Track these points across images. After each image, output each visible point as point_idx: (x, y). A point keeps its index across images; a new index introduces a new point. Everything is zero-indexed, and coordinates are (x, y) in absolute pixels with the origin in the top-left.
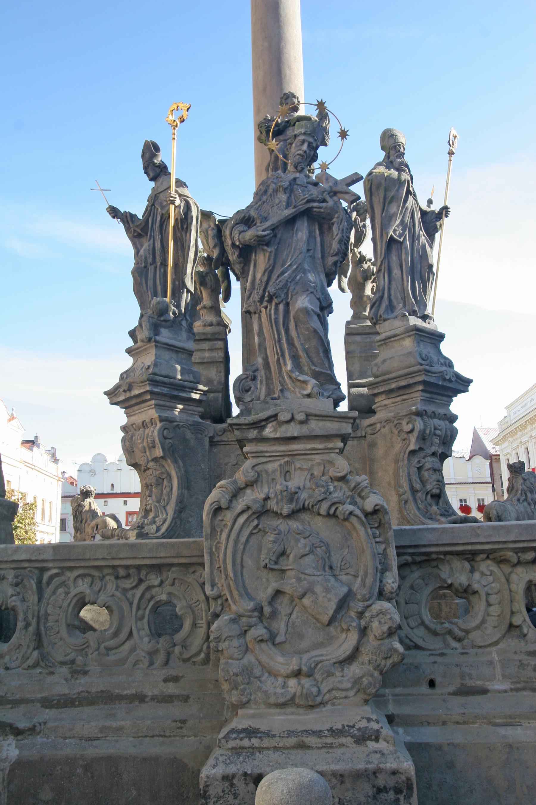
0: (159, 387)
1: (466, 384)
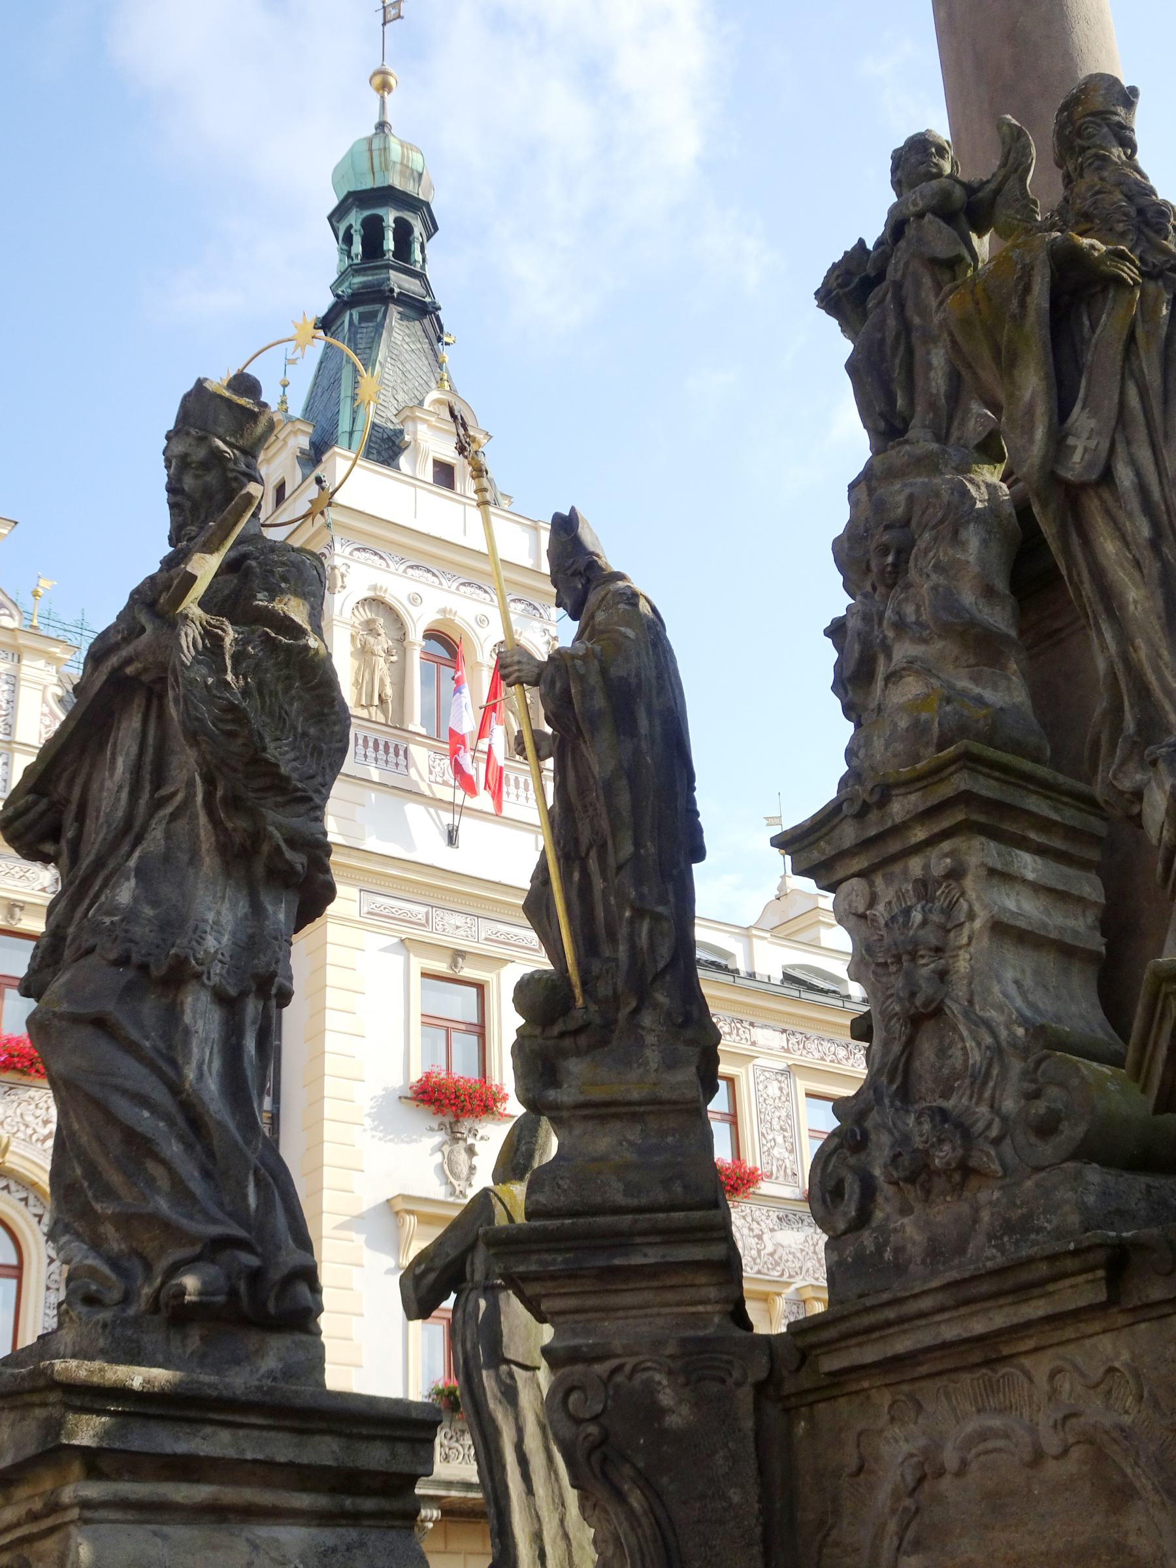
0: (535, 1257)
1: (422, 1435)
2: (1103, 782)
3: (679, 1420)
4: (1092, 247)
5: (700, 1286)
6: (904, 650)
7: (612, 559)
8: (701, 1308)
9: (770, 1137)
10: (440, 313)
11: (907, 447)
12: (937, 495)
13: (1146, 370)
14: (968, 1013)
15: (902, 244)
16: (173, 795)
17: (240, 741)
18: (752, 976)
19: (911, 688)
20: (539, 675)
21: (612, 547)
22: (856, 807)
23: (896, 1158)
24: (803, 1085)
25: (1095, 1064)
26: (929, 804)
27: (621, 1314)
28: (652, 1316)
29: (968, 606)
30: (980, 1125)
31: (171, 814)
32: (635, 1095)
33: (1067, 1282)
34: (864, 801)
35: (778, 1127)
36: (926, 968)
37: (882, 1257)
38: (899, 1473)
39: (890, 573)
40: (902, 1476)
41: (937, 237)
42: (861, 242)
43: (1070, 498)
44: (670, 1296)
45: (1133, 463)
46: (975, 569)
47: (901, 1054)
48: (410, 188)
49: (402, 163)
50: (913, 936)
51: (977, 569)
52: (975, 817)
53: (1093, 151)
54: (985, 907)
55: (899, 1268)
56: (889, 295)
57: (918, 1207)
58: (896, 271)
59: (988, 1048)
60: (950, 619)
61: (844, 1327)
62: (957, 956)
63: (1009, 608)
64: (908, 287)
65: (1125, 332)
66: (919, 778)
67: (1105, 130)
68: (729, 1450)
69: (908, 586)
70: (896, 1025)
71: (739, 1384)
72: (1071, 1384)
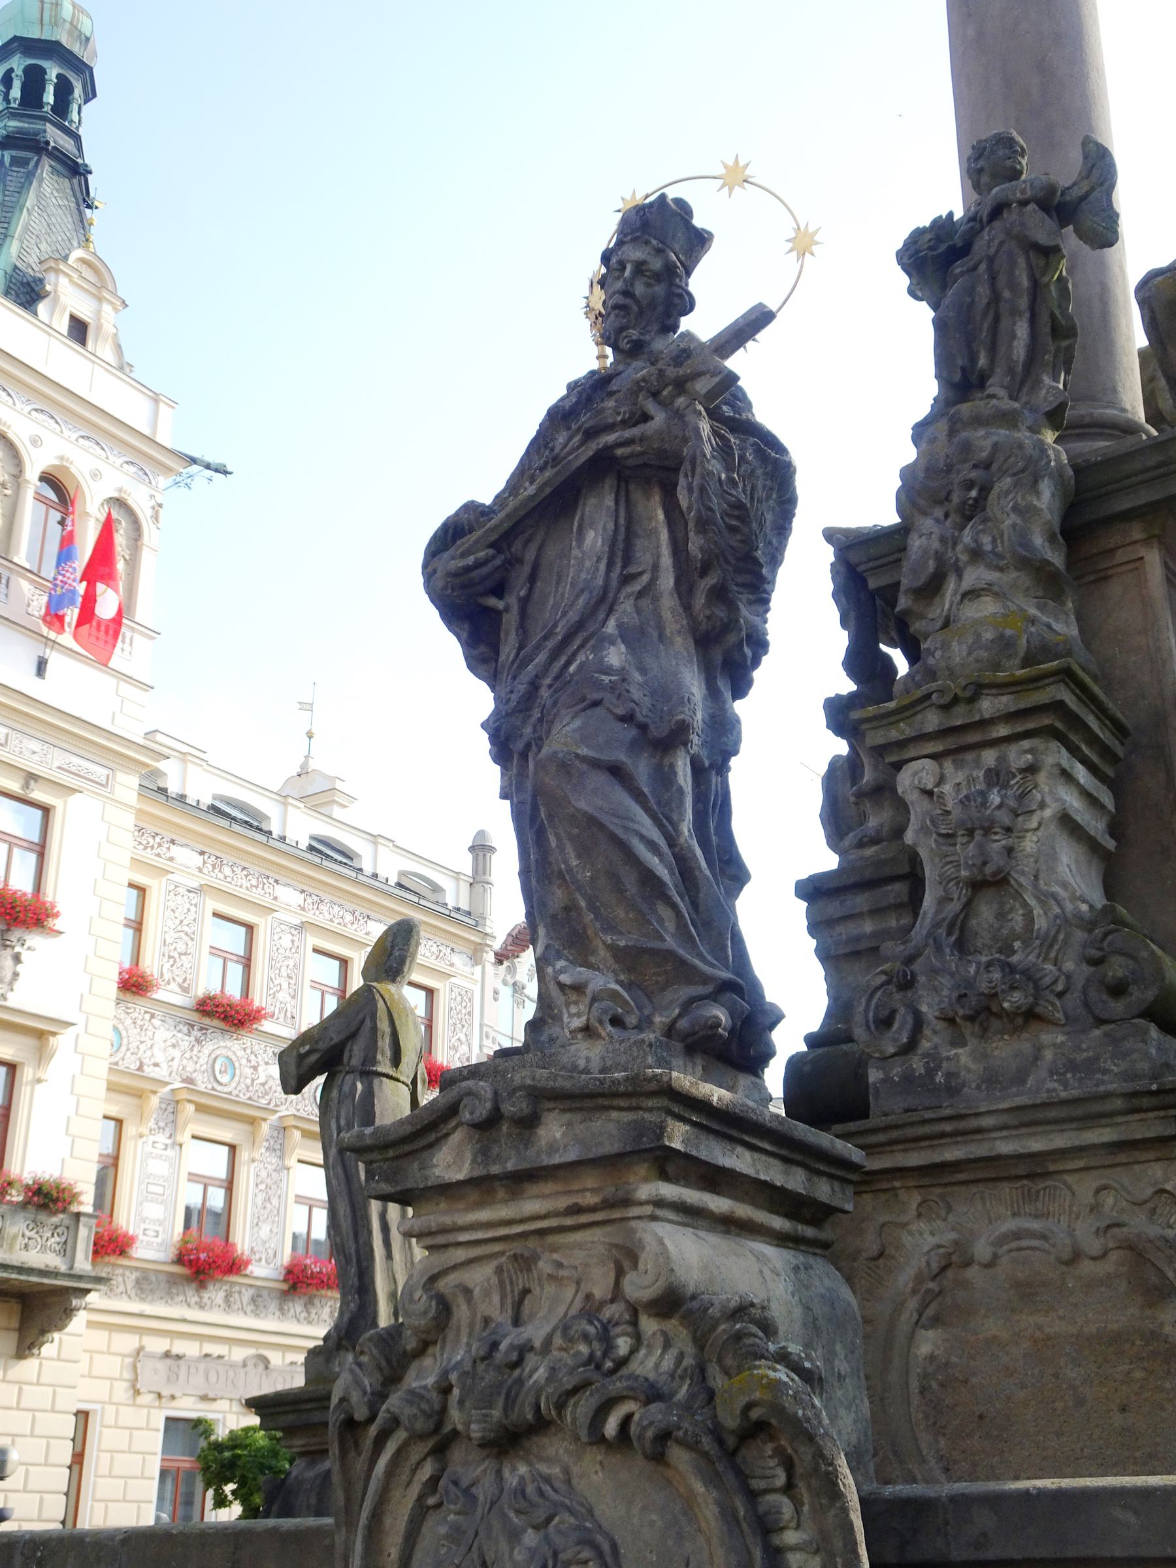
6: (974, 576)
9: (276, 982)
10: (90, 177)
11: (994, 401)
15: (997, 224)
16: (640, 574)
17: (739, 537)
18: (283, 839)
19: (988, 607)
22: (947, 699)
24: (312, 940)
26: (1022, 706)
30: (1047, 980)
31: (639, 592)
35: (285, 974)
39: (971, 506)
42: (951, 214)
48: (76, 49)
49: (71, 23)
61: (894, 1134)
62: (1024, 837)
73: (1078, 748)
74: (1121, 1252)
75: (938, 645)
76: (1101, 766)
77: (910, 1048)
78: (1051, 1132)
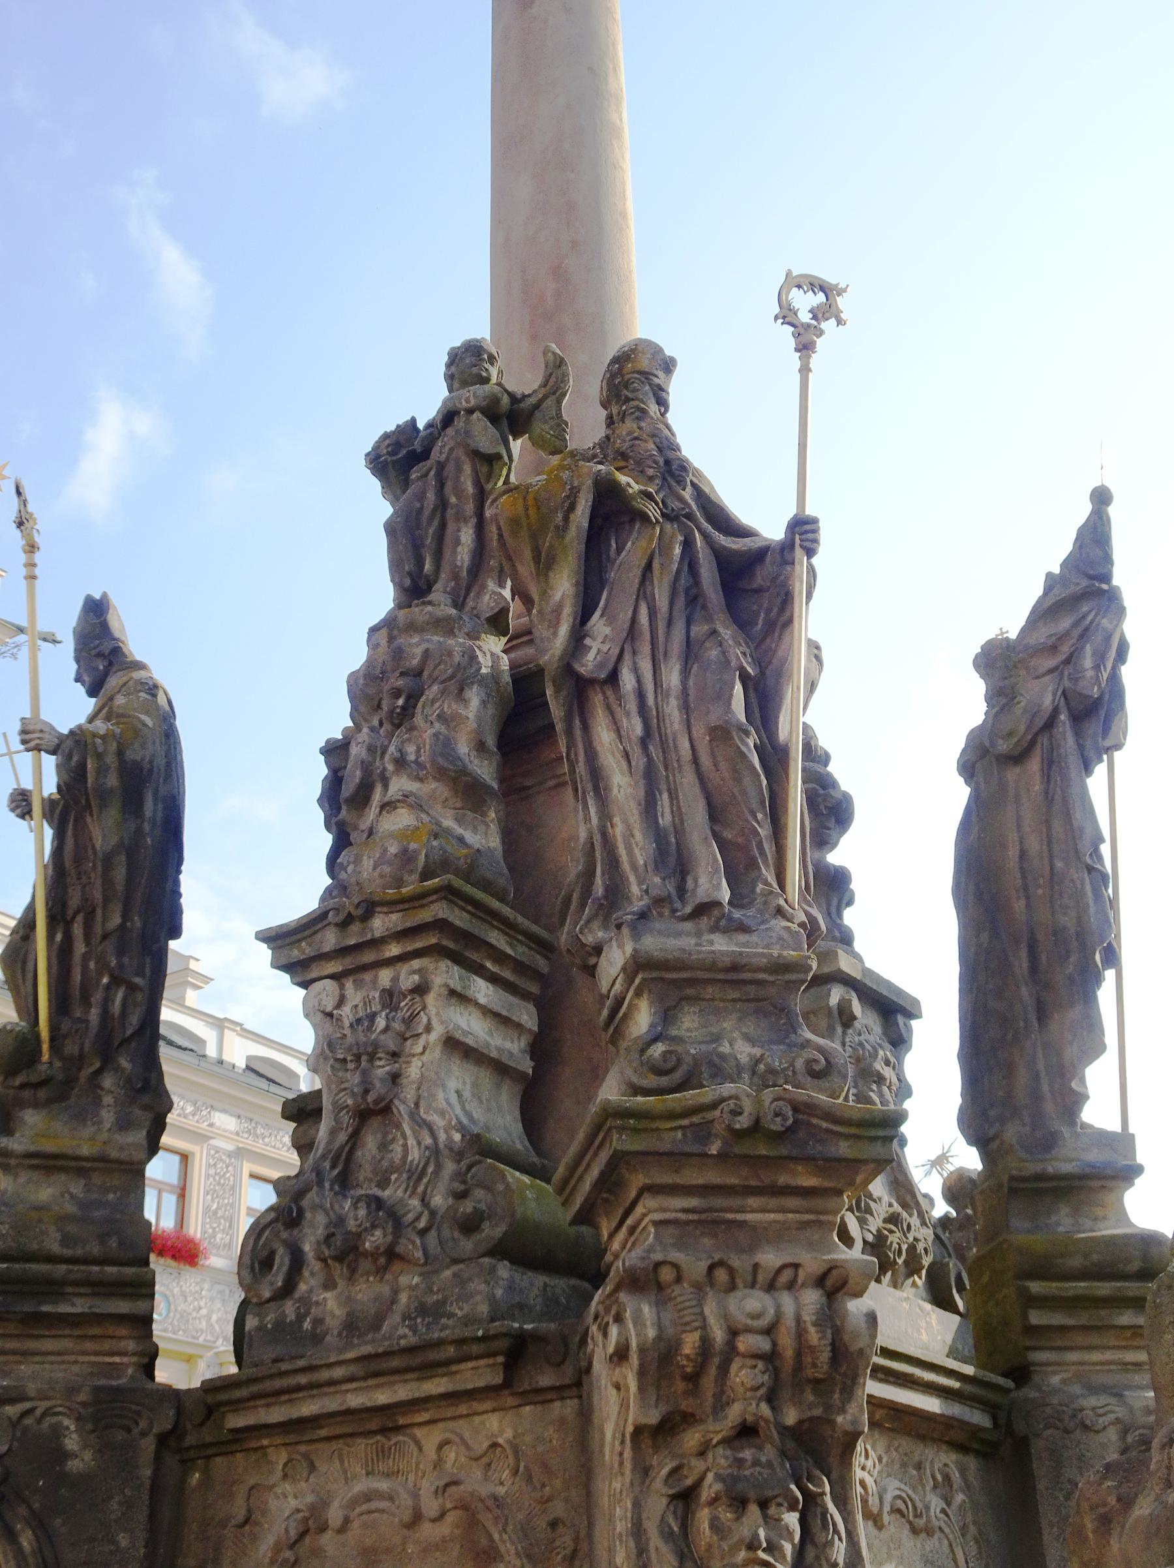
2: (568, 933)
3: (81, 1465)
4: (628, 484)
5: (120, 1338)
6: (400, 784)
7: (137, 647)
8: (117, 1359)
11: (429, 608)
12: (450, 654)
13: (657, 597)
14: (414, 1115)
15: (450, 431)
19: (402, 819)
20: (58, 746)
21: (138, 638)
22: (341, 917)
23: (328, 1238)
25: (517, 1174)
26: (408, 925)
27: (37, 1358)
28: (69, 1362)
29: (462, 756)
30: (411, 1217)
32: (85, 1151)
33: (470, 1365)
34: (349, 913)
36: (382, 1069)
37: (301, 1327)
38: (283, 1526)
40: (287, 1530)
41: (484, 436)
43: (580, 689)
44: (89, 1345)
45: (636, 670)
46: (472, 724)
47: (347, 1143)
50: (375, 1039)
51: (474, 725)
52: (445, 942)
53: (633, 403)
54: (442, 1023)
55: (316, 1338)
56: (432, 473)
57: (341, 1284)
58: (441, 453)
59: (427, 1148)
60: (446, 765)
61: (255, 1388)
63: (495, 764)
64: (450, 469)
65: (645, 561)
66: (403, 901)
67: (647, 387)
68: (125, 1496)
69: (412, 728)
70: (345, 1118)
71: (144, 1434)
72: (457, 1454)
73: (482, 967)
74: (458, 1512)
75: (351, 859)
76: (518, 983)
77: (288, 1289)
78: (393, 1383)
